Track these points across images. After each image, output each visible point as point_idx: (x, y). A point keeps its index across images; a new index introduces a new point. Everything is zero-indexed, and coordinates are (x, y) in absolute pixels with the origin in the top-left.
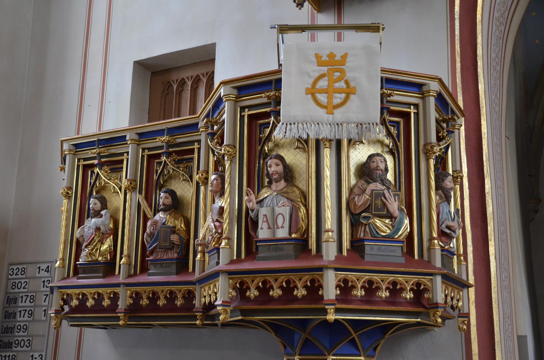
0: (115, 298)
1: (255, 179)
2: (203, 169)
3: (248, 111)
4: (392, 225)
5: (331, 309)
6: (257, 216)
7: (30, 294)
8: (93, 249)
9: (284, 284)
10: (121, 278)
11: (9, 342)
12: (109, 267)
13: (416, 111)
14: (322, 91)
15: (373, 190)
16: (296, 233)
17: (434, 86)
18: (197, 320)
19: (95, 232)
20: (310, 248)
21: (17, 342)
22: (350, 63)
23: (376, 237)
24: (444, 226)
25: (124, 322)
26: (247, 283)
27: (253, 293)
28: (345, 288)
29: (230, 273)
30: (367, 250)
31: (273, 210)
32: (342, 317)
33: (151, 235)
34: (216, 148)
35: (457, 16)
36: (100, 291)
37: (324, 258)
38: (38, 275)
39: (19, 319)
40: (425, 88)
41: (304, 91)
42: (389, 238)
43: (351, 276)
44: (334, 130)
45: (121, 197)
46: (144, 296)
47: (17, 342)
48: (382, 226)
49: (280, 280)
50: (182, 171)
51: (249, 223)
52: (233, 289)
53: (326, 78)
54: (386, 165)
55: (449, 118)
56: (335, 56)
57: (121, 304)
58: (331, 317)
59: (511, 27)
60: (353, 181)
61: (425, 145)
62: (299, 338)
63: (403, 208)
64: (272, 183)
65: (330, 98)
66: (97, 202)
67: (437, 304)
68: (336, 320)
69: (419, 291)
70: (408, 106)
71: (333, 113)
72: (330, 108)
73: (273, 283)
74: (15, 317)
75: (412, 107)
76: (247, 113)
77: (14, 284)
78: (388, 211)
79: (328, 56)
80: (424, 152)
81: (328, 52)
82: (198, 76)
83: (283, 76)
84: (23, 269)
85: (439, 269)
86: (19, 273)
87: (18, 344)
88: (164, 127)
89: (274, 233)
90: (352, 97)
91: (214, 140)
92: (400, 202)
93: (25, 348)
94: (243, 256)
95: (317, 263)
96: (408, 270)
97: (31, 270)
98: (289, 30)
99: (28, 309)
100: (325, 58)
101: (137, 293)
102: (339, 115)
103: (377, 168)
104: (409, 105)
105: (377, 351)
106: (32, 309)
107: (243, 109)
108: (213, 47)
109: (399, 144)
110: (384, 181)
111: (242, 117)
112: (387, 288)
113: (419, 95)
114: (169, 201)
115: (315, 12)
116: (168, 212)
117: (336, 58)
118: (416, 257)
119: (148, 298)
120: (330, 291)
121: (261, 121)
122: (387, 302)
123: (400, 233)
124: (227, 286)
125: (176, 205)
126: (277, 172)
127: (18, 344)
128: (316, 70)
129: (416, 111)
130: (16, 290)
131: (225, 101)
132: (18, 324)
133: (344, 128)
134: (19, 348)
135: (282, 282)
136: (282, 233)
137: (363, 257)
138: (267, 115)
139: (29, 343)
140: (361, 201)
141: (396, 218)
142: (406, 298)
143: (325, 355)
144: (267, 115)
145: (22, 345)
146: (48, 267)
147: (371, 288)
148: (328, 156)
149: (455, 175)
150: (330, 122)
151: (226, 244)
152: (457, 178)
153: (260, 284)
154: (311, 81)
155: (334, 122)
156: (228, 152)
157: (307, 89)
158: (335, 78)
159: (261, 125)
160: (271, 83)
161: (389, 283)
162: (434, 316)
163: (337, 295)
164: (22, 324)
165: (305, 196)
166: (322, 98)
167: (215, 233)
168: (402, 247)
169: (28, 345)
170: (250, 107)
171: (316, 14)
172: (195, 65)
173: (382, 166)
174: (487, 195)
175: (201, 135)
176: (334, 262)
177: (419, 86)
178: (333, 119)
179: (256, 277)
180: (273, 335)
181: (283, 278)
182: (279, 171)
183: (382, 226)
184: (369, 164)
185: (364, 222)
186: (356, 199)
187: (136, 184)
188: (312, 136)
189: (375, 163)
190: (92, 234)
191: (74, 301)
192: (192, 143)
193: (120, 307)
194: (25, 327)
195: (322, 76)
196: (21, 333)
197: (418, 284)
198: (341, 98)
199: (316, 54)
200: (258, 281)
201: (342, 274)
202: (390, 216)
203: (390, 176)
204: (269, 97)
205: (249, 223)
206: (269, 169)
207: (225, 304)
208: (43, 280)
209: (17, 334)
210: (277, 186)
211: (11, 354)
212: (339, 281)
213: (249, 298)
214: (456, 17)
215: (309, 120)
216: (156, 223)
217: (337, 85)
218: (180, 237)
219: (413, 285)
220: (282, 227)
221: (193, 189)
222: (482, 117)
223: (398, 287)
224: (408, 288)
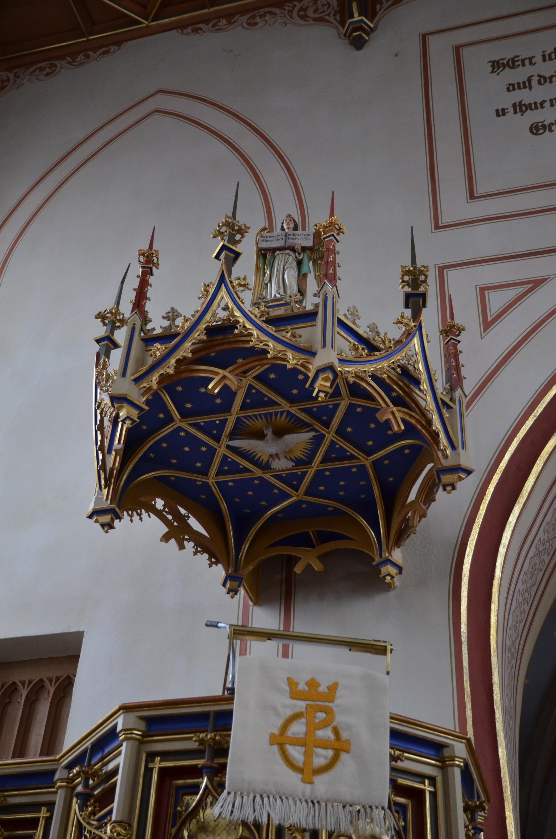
3: (161, 761)
13: (432, 789)
14: (296, 742)
22: (342, 699)
34: (88, 823)
35: (464, 639)
40: (446, 752)
41: (267, 739)
44: (312, 813)
53: (304, 720)
55: (476, 806)
56: (319, 685)
59: (522, 662)
65: (308, 755)
70: (420, 780)
71: (311, 783)
72: (308, 772)
75: (427, 782)
76: (157, 764)
79: (307, 684)
81: (307, 678)
82: (41, 680)
83: (236, 708)
90: (344, 756)
91: (87, 807)
98: (247, 635)
102: (322, 785)
104: (421, 777)
107: (151, 756)
108: (78, 637)
111: (148, 772)
113: (438, 763)
115: (250, 603)
121: (180, 782)
128: (289, 705)
129: (432, 789)
131: (123, 740)
138: (196, 772)
144: (196, 772)
150: (307, 796)
154: (279, 722)
155: (313, 798)
157: (272, 735)
158: (317, 721)
159: (180, 788)
160: (211, 719)
166: (296, 753)
170: (165, 755)
171: (251, 607)
172: (37, 662)
175: (56, 793)
178: (312, 792)
192: (36, 807)
195: (296, 717)
198: (325, 757)
199: (288, 679)
204: (202, 742)
214: (463, 639)
215: (273, 790)
217: (320, 733)
222: (506, 804)
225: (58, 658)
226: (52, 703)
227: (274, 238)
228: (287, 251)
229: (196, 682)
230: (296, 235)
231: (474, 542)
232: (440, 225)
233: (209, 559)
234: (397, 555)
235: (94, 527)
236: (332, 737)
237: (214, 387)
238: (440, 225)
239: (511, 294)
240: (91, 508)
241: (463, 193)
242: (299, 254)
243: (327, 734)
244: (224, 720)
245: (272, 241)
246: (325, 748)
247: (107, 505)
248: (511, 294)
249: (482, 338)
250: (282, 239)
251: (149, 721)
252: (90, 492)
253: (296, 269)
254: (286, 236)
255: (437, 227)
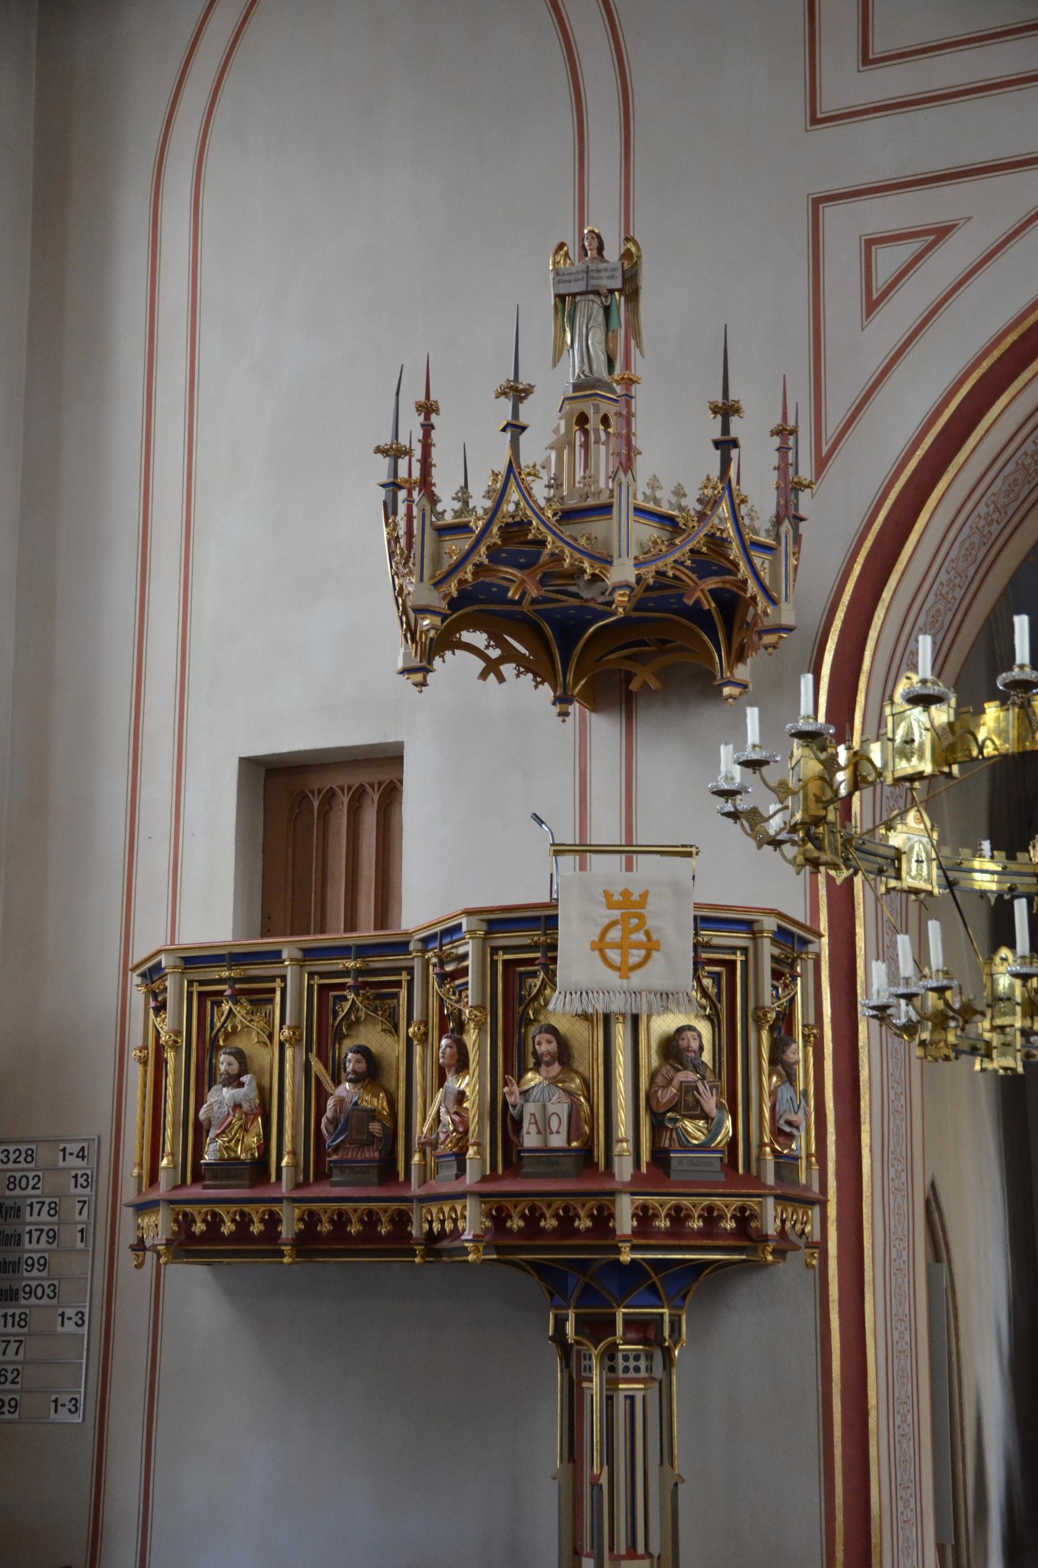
0: (273, 1221)
1: (513, 1058)
2: (420, 1018)
4: (707, 1128)
5: (625, 1247)
6: (521, 1114)
7: (48, 1201)
8: (229, 1141)
9: (561, 1212)
10: (284, 1189)
11: (12, 1290)
12: (258, 1170)
13: (743, 958)
14: (614, 946)
15: (682, 1082)
16: (577, 1140)
17: (770, 924)
18: (416, 1256)
19: (234, 1111)
20: (596, 1160)
21: (27, 1289)
22: (653, 905)
23: (686, 1147)
24: (782, 1122)
25: (290, 1260)
26: (507, 1209)
27: (516, 1223)
28: (644, 1216)
29: (483, 1196)
30: (674, 1164)
31: (544, 1107)
32: (640, 1256)
33: (334, 1121)
36: (246, 1209)
37: (617, 1178)
38: (61, 1164)
39: (27, 1246)
40: (756, 927)
42: (704, 1147)
43: (653, 1200)
45: (271, 1047)
46: (325, 1218)
47: (27, 1289)
48: (694, 1129)
49: (554, 1206)
50: (382, 1016)
51: (506, 1123)
52: (487, 1218)
53: (619, 927)
54: (701, 1041)
57: (287, 1230)
58: (626, 1257)
60: (655, 1061)
61: (757, 1008)
62: (575, 1283)
63: (724, 1102)
64: (540, 1065)
65: (624, 956)
66: (232, 1059)
67: (767, 1236)
68: (633, 1260)
69: (744, 1218)
71: (628, 978)
72: (624, 970)
73: (545, 1210)
74: (19, 1243)
77: (12, 1180)
78: (702, 1109)
79: (621, 894)
80: (754, 1020)
81: (621, 889)
82: (362, 786)
84: (29, 1152)
85: (771, 1188)
86: (21, 1159)
87: (30, 1293)
88: (351, 942)
89: (546, 1140)
90: (655, 955)
92: (720, 1094)
93: (45, 1300)
94: (500, 1171)
95: (607, 1186)
96: (728, 1191)
97: (43, 1153)
99: (46, 1228)
100: (617, 897)
101: (311, 1213)
102: (637, 980)
103: (688, 1049)
104: (733, 949)
105: (687, 1302)
106: (56, 1228)
107: (495, 950)
109: (719, 1005)
110: (697, 1067)
111: (494, 963)
112: (700, 1216)
114: (362, 1066)
116: (360, 1085)
117: (633, 898)
118: (741, 1171)
119: (331, 1221)
120: (625, 1223)
122: (701, 1234)
123: (719, 1138)
124: (478, 1213)
125: (372, 1072)
126: (549, 1053)
127: (30, 1293)
128: (607, 915)
130: (18, 1192)
132: (26, 1255)
133: (644, 999)
134: (33, 1300)
135: (558, 1209)
136: (558, 1141)
137: (668, 1175)
139: (53, 1291)
140: (666, 1096)
141: (712, 1119)
142: (725, 1229)
143: (613, 1307)
145: (39, 1294)
146: (83, 1149)
147: (678, 1216)
148: (621, 1034)
149: (807, 1032)
150: (625, 988)
151: (476, 1153)
152: (809, 1036)
153: (527, 1211)
154: (598, 931)
156: (476, 1016)
157: (593, 943)
159: (521, 974)
160: (543, 920)
161: (702, 1209)
162: (763, 1253)
163: (633, 1228)
164: (36, 1256)
165: (587, 1084)
166: (614, 955)
167: (454, 1131)
168: (721, 1158)
169: (52, 1295)
170: (506, 949)
173: (695, 1045)
174: (861, 1050)
176: (630, 1183)
177: (748, 926)
179: (521, 1202)
180: (536, 1278)
181: (559, 1202)
182: (551, 1050)
183: (694, 1129)
184: (677, 1042)
185: (670, 1126)
186: (660, 1093)
187: (301, 1035)
188: (600, 1011)
189: (685, 1041)
190: (228, 1115)
191: (199, 1224)
192: (397, 971)
193: (284, 1236)
194: (42, 1261)
195: (613, 924)
196: (35, 1273)
197: (742, 1209)
198: (639, 956)
199: (604, 891)
200: (524, 1207)
201: (641, 1199)
202: (705, 1116)
203: (707, 1057)
205: (506, 1123)
206: (537, 1047)
207: (476, 1239)
208: (73, 1173)
209: (26, 1274)
210: (548, 1072)
211: (18, 1312)
212: (637, 1208)
213: (511, 1230)
215: (596, 987)
216: (341, 1101)
218: (384, 1125)
219: (735, 1210)
220: (558, 1132)
221: (402, 1047)
223: (715, 1214)
224: (729, 1216)
225: (377, 759)
226: (378, 812)
227: (572, 277)
228: (591, 297)
229: (524, 891)
230: (599, 271)
231: (837, 633)
232: (819, 116)
233: (535, 680)
234: (742, 672)
235: (406, 683)
236: (644, 938)
237: (514, 594)
238: (819, 116)
239: (906, 251)
240: (400, 665)
241: (853, 51)
242: (606, 297)
243: (640, 936)
244: (552, 922)
245: (570, 281)
246: (639, 949)
247: (416, 662)
248: (906, 251)
249: (863, 329)
250: (583, 279)
251: (490, 922)
252: (398, 652)
253: (603, 328)
254: (587, 272)
255: (815, 121)
